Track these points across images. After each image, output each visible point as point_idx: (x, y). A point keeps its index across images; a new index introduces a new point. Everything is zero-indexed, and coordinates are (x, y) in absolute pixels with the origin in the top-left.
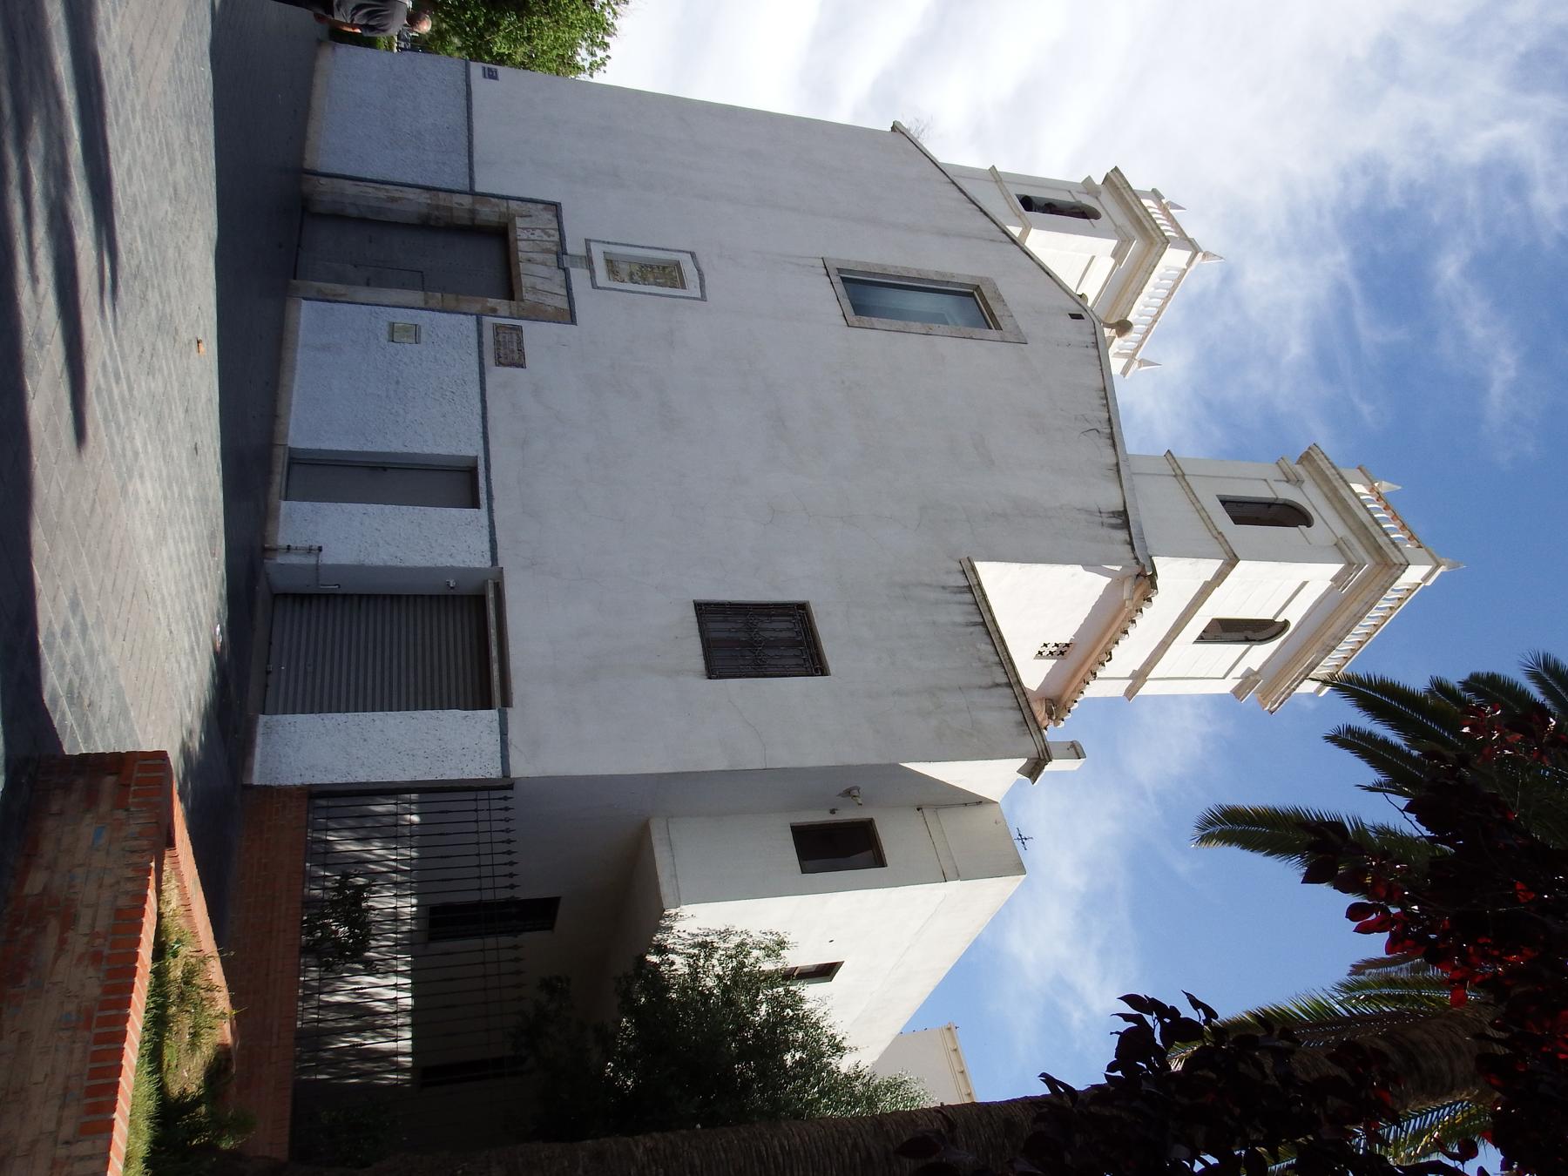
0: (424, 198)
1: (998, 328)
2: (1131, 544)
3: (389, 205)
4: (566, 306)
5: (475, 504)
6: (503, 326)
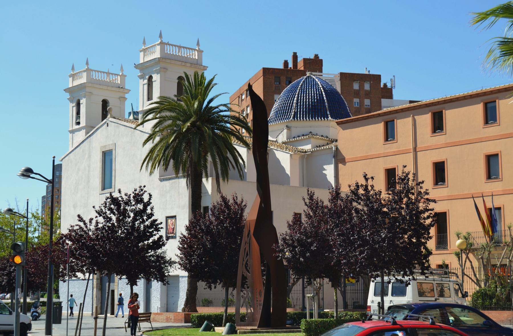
0: (95, 290)
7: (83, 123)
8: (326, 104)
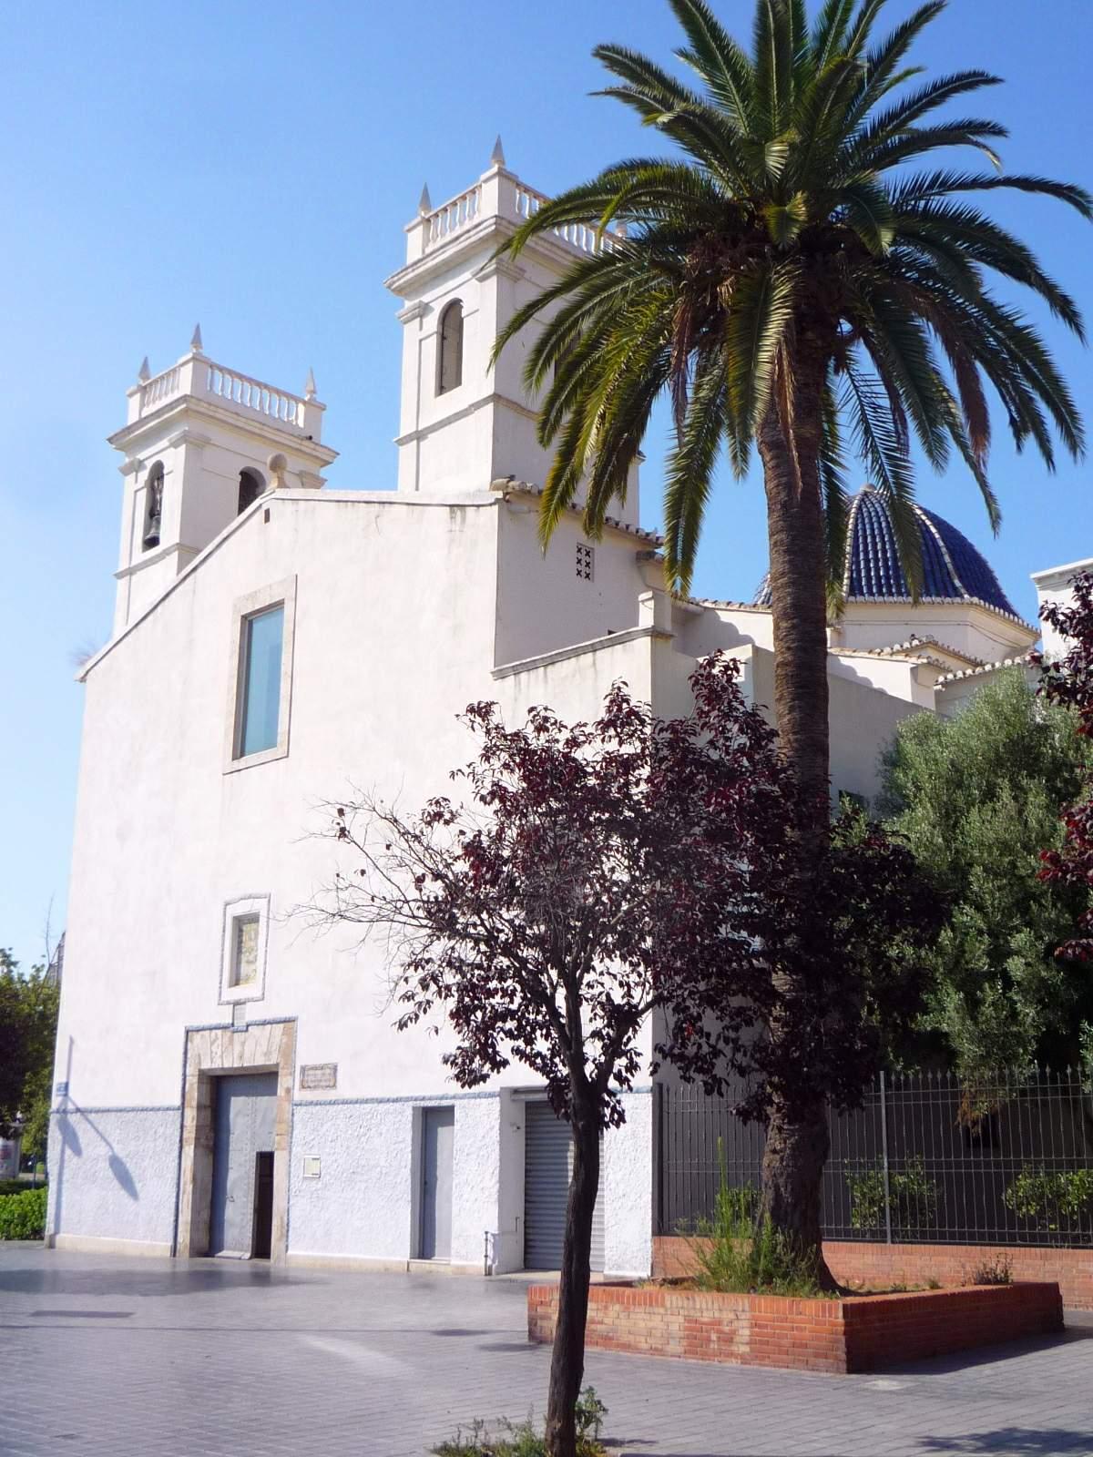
0: (189, 1150)
1: (278, 605)
2: (478, 506)
3: (199, 1182)
4: (282, 1025)
5: (451, 1109)
6: (302, 1081)
7: (170, 532)
8: (947, 558)
